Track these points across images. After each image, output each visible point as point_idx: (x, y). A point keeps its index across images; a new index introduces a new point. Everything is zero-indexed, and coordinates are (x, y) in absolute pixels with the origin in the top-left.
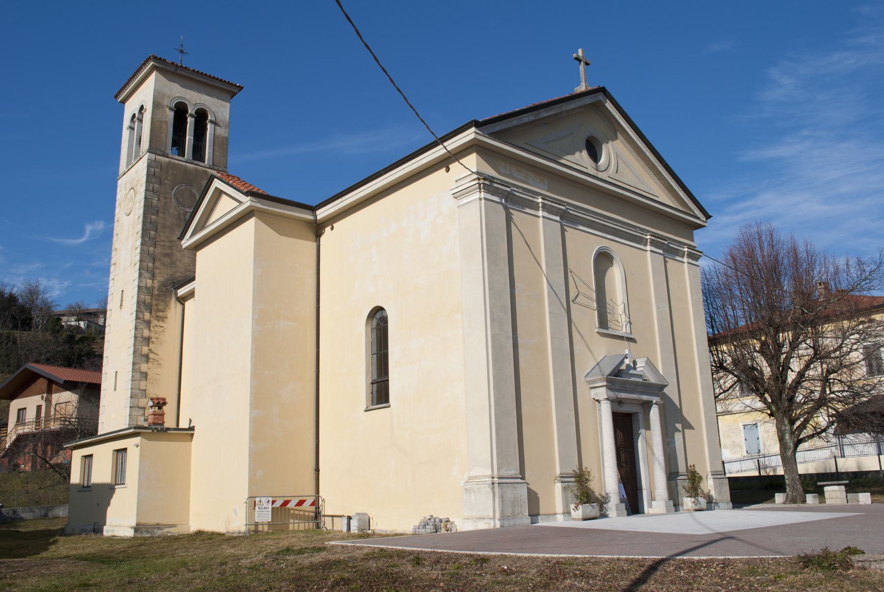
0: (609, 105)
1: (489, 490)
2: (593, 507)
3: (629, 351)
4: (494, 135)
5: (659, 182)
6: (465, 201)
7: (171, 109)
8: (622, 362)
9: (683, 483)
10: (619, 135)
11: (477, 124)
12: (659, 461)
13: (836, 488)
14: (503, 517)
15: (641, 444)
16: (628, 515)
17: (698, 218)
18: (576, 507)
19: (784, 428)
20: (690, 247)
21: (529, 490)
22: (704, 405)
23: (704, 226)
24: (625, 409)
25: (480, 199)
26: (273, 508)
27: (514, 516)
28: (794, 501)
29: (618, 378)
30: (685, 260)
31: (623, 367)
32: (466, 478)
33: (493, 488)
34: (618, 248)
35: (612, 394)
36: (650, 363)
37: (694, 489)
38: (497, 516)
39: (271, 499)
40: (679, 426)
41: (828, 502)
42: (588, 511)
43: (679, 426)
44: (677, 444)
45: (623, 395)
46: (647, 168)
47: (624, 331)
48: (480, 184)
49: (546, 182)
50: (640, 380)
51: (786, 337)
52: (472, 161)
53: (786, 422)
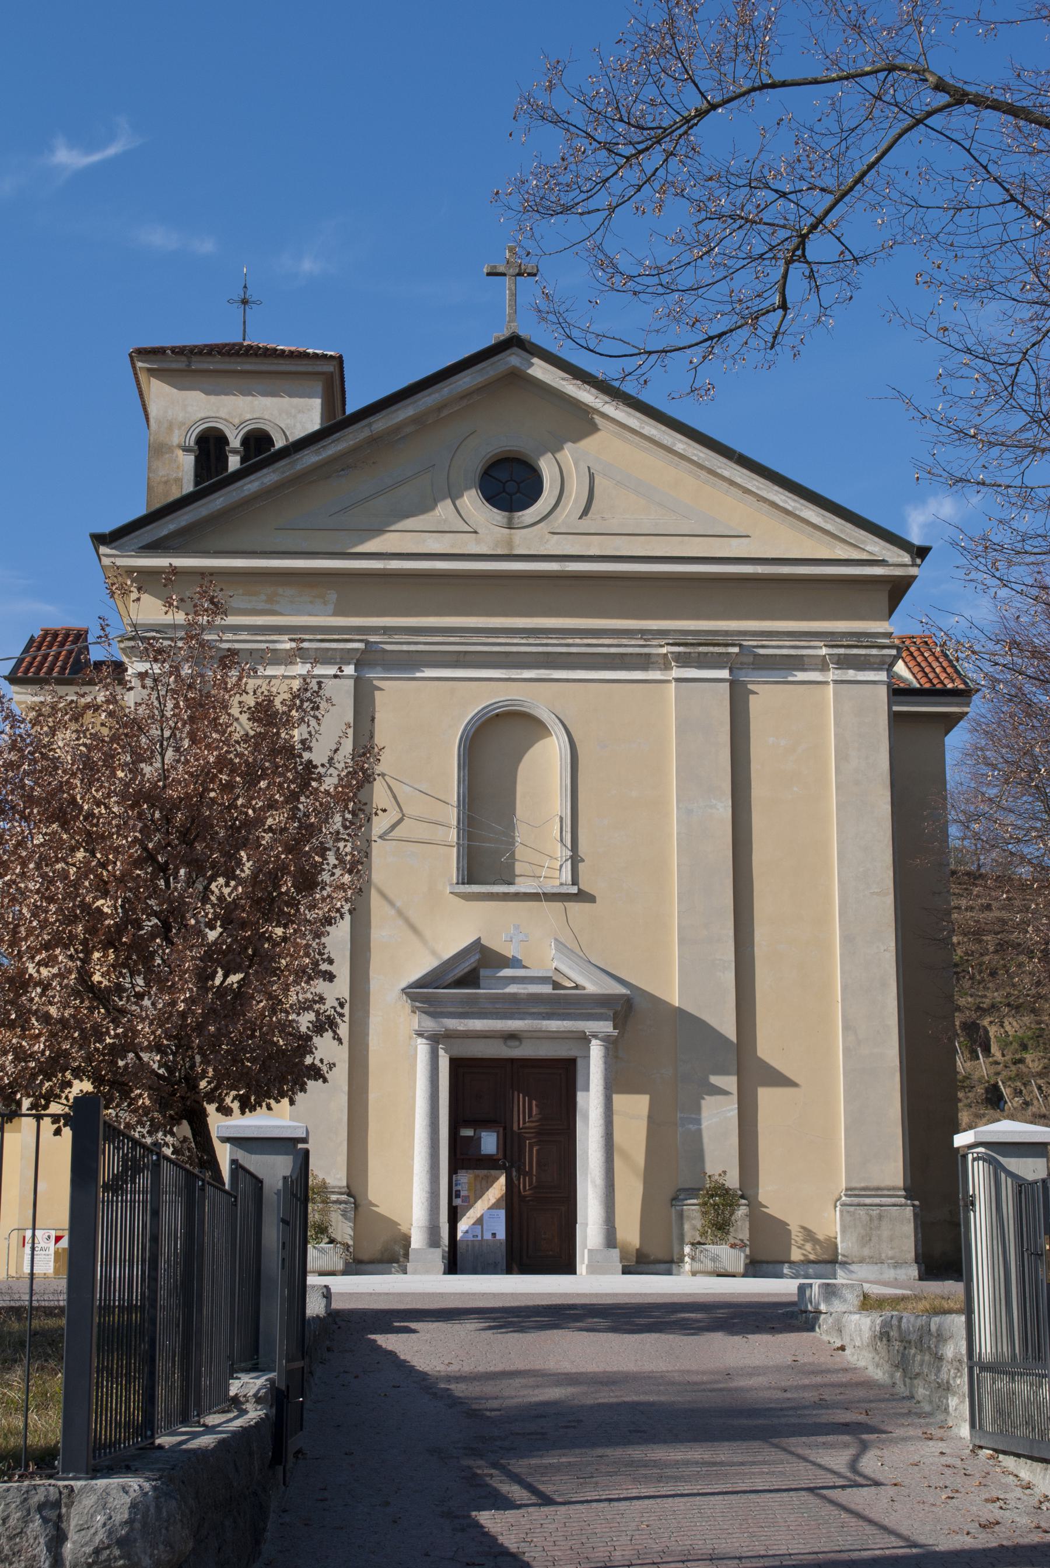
0: (540, 370)
7: (186, 450)
16: (444, 1273)
17: (882, 563)
26: (56, 1253)
35: (430, 1024)
39: (53, 1234)
50: (547, 989)
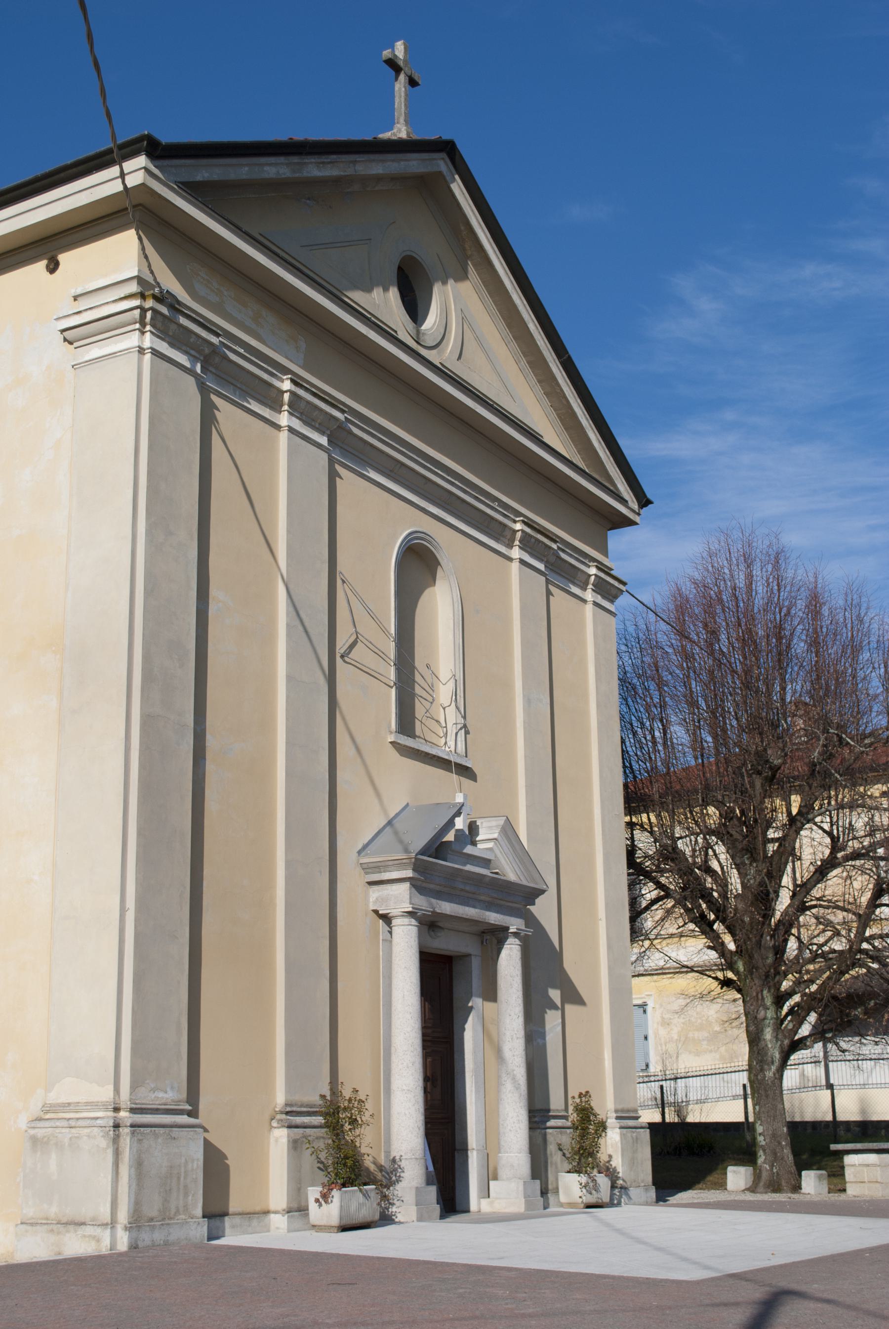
1: (103, 1142)
2: (366, 1195)
3: (465, 797)
4: (193, 190)
5: (546, 402)
6: (95, 352)
8: (450, 823)
9: (559, 1138)
10: (471, 269)
11: (155, 150)
12: (514, 1078)
13: (872, 1158)
14: (136, 1223)
15: (471, 1036)
17: (623, 501)
18: (325, 1197)
19: (762, 1014)
20: (601, 567)
21: (207, 1144)
22: (609, 947)
23: (632, 523)
24: (445, 944)
25: (141, 351)
27: (165, 1218)
28: (775, 1187)
29: (440, 862)
30: (589, 595)
31: (450, 837)
32: (35, 1107)
33: (116, 1140)
34: (452, 543)
35: (424, 903)
36: (509, 830)
37: (585, 1157)
38: (123, 1216)
40: (555, 995)
41: (852, 1190)
42: (354, 1206)
43: (555, 995)
44: (549, 1038)
45: (447, 907)
46: (524, 362)
47: (449, 746)
48: (144, 311)
49: (303, 345)
51: (785, 806)
52: (119, 256)
53: (769, 1001)
